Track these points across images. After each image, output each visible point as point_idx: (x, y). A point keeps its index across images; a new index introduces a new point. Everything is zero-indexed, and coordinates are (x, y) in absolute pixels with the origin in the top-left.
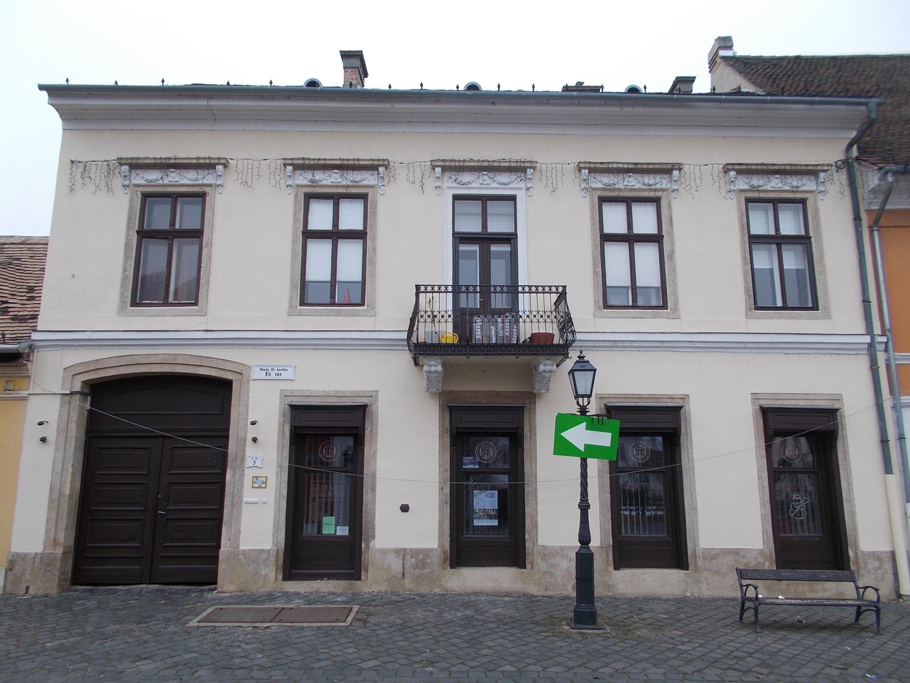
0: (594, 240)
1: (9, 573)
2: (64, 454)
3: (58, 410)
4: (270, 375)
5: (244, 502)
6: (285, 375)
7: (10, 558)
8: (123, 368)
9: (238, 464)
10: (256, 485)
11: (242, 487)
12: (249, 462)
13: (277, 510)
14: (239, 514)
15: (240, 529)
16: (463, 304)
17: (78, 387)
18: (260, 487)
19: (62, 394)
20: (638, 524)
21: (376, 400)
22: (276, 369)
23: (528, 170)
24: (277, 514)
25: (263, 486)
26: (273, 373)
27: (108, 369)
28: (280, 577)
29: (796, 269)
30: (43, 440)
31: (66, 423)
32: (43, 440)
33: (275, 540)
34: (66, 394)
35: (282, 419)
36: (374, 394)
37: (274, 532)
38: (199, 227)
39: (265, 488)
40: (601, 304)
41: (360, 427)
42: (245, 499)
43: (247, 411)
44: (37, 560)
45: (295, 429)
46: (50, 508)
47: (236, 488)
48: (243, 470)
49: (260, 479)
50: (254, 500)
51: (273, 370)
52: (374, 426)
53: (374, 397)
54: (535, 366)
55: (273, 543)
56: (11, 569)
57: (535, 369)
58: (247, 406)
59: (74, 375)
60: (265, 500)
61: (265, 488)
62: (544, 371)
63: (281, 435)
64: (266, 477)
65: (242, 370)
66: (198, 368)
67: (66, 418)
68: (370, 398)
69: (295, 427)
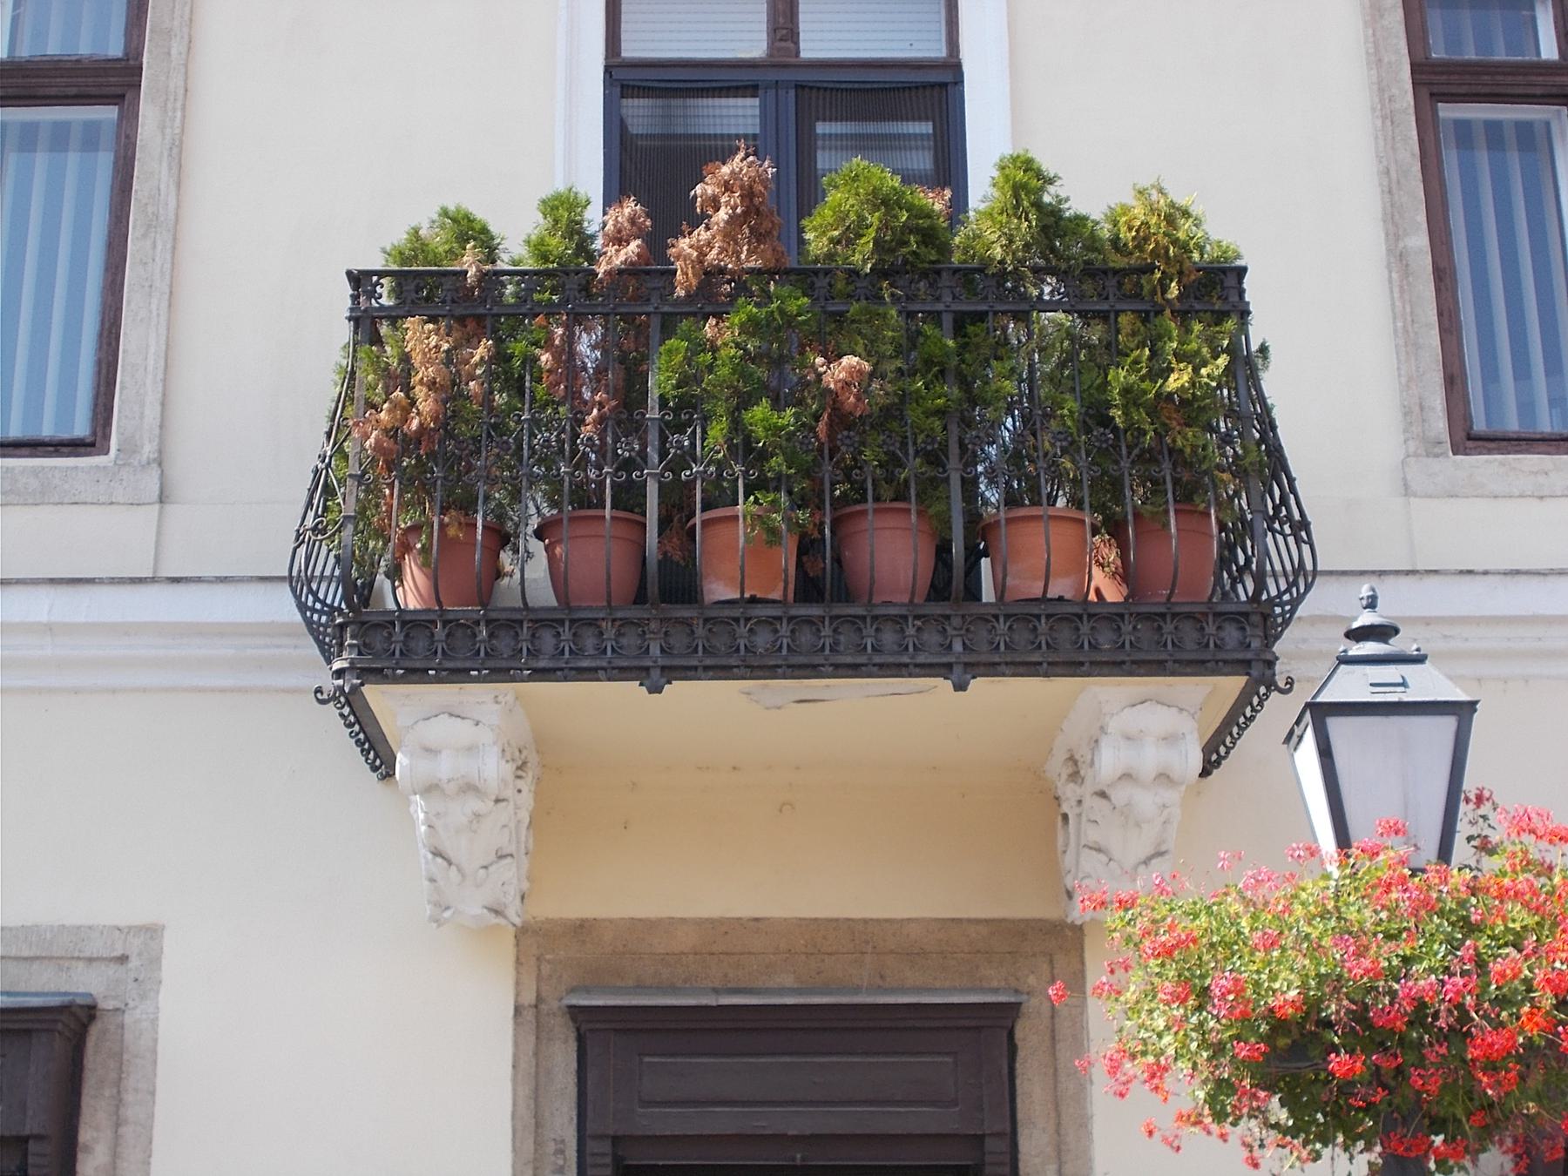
0: (1382, 89)
20: (836, 107)
21: (148, 985)
29: (1489, 148)
36: (134, 945)
38: (115, 49)
40: (1439, 425)
41: (39, 1138)
52: (127, 1131)
53: (134, 963)
54: (1072, 760)
57: (1075, 776)
62: (1127, 776)
68: (112, 971)
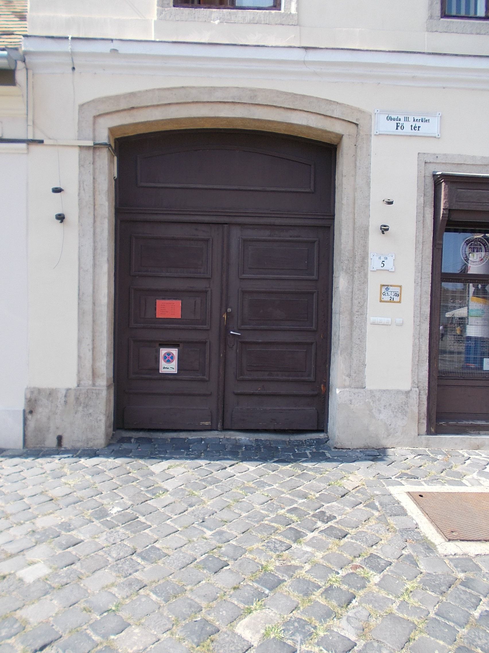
1: (29, 417)
2: (94, 242)
3: (77, 172)
4: (402, 128)
5: (368, 323)
6: (425, 129)
7: (29, 396)
8: (173, 108)
9: (358, 265)
10: (387, 298)
11: (365, 300)
12: (374, 263)
13: (418, 336)
14: (362, 339)
15: (364, 361)
16: (441, 366)
17: (104, 137)
18: (392, 301)
19: (80, 147)
22: (411, 119)
23: (305, 626)
24: (417, 341)
25: (396, 299)
26: (407, 126)
27: (149, 110)
28: (424, 428)
30: (61, 218)
31: (91, 194)
32: (61, 218)
33: (416, 378)
34: (88, 147)
35: (422, 198)
37: (413, 366)
39: (400, 302)
42: (371, 318)
43: (368, 184)
44: (72, 399)
45: (449, 214)
46: (81, 324)
47: (356, 302)
48: (366, 275)
49: (391, 289)
50: (385, 320)
51: (407, 119)
55: (413, 382)
56: (31, 412)
58: (369, 178)
59: (95, 117)
60: (399, 320)
61: (400, 302)
63: (421, 224)
64: (400, 287)
65: (357, 120)
66: (289, 114)
67: (92, 186)
69: (450, 210)
